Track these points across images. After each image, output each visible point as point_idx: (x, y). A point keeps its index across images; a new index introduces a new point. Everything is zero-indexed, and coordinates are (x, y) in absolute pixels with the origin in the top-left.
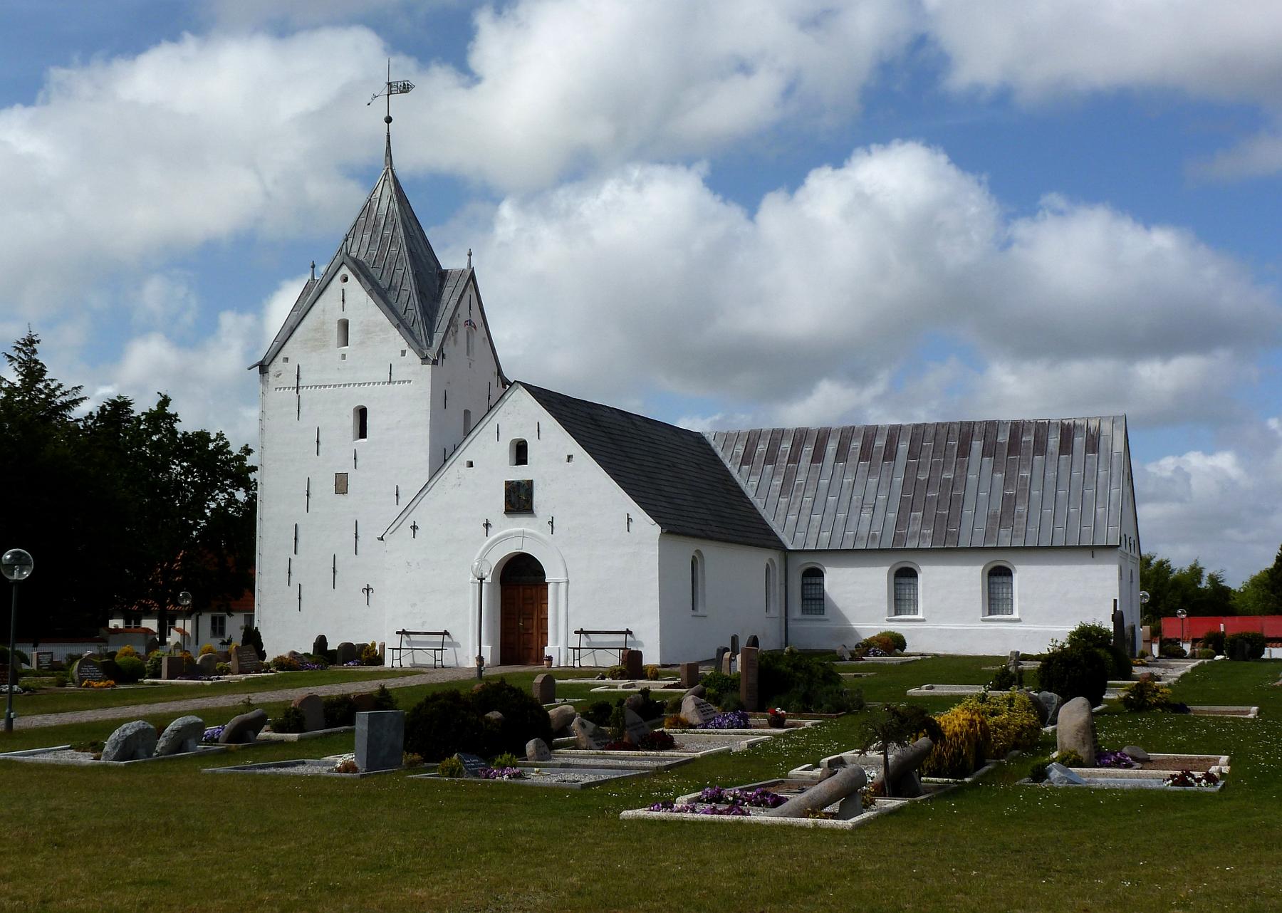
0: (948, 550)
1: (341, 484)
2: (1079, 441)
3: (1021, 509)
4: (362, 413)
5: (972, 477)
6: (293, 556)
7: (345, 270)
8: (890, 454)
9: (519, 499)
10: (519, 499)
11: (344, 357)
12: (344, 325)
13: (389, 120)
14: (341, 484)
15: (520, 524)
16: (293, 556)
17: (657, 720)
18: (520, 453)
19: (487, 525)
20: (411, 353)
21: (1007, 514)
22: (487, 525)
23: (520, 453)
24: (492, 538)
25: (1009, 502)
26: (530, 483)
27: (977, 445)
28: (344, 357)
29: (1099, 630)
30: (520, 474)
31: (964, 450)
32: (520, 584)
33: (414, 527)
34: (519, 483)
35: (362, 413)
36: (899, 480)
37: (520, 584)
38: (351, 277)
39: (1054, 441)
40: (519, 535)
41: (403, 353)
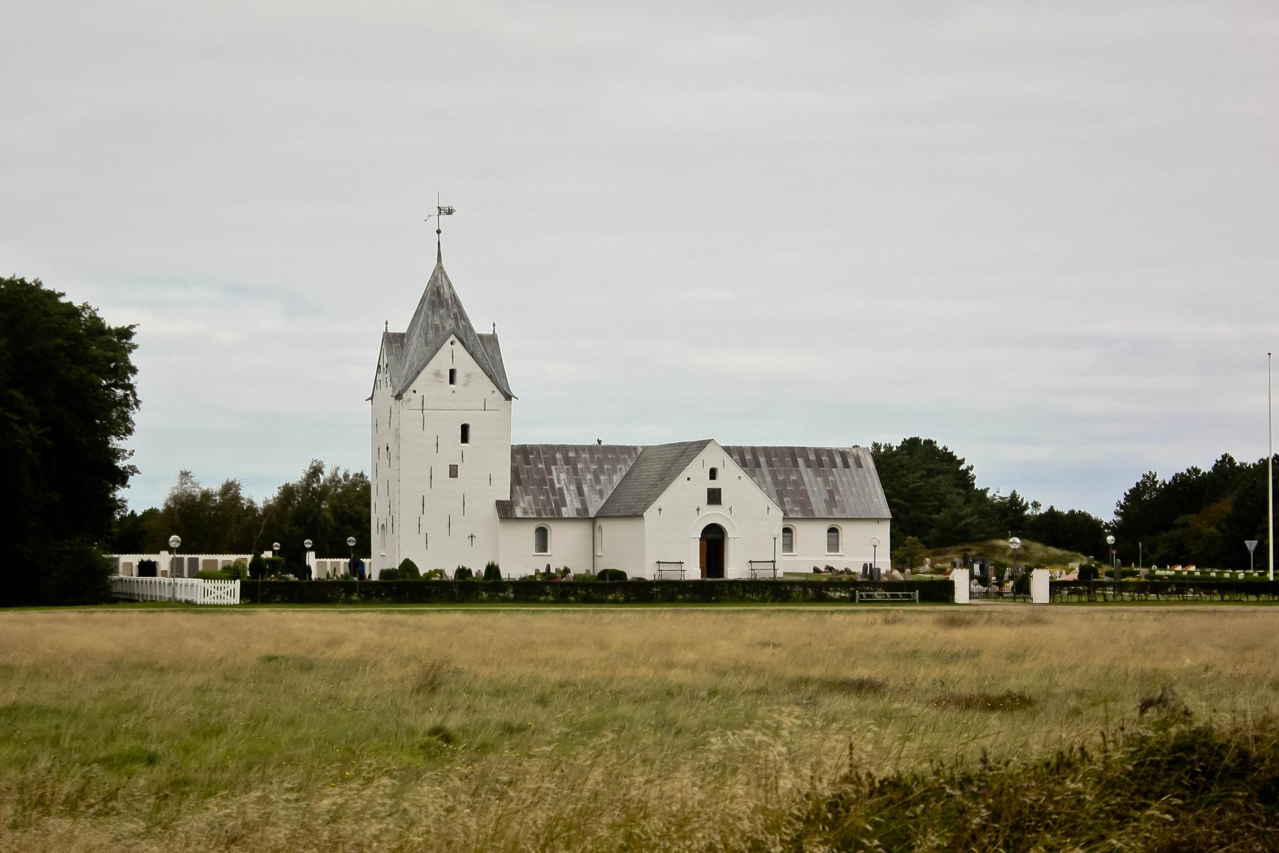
0: (810, 517)
1: (453, 471)
2: (851, 461)
3: (837, 498)
4: (465, 429)
5: (806, 479)
7: (453, 338)
8: (758, 465)
9: (714, 497)
10: (714, 497)
12: (452, 372)
13: (439, 232)
14: (453, 471)
15: (715, 509)
18: (713, 474)
20: (497, 392)
21: (831, 502)
23: (713, 474)
25: (831, 493)
27: (800, 461)
29: (416, 570)
31: (796, 465)
32: (713, 541)
35: (465, 429)
36: (769, 479)
37: (713, 541)
38: (457, 342)
39: (838, 460)
40: (714, 515)
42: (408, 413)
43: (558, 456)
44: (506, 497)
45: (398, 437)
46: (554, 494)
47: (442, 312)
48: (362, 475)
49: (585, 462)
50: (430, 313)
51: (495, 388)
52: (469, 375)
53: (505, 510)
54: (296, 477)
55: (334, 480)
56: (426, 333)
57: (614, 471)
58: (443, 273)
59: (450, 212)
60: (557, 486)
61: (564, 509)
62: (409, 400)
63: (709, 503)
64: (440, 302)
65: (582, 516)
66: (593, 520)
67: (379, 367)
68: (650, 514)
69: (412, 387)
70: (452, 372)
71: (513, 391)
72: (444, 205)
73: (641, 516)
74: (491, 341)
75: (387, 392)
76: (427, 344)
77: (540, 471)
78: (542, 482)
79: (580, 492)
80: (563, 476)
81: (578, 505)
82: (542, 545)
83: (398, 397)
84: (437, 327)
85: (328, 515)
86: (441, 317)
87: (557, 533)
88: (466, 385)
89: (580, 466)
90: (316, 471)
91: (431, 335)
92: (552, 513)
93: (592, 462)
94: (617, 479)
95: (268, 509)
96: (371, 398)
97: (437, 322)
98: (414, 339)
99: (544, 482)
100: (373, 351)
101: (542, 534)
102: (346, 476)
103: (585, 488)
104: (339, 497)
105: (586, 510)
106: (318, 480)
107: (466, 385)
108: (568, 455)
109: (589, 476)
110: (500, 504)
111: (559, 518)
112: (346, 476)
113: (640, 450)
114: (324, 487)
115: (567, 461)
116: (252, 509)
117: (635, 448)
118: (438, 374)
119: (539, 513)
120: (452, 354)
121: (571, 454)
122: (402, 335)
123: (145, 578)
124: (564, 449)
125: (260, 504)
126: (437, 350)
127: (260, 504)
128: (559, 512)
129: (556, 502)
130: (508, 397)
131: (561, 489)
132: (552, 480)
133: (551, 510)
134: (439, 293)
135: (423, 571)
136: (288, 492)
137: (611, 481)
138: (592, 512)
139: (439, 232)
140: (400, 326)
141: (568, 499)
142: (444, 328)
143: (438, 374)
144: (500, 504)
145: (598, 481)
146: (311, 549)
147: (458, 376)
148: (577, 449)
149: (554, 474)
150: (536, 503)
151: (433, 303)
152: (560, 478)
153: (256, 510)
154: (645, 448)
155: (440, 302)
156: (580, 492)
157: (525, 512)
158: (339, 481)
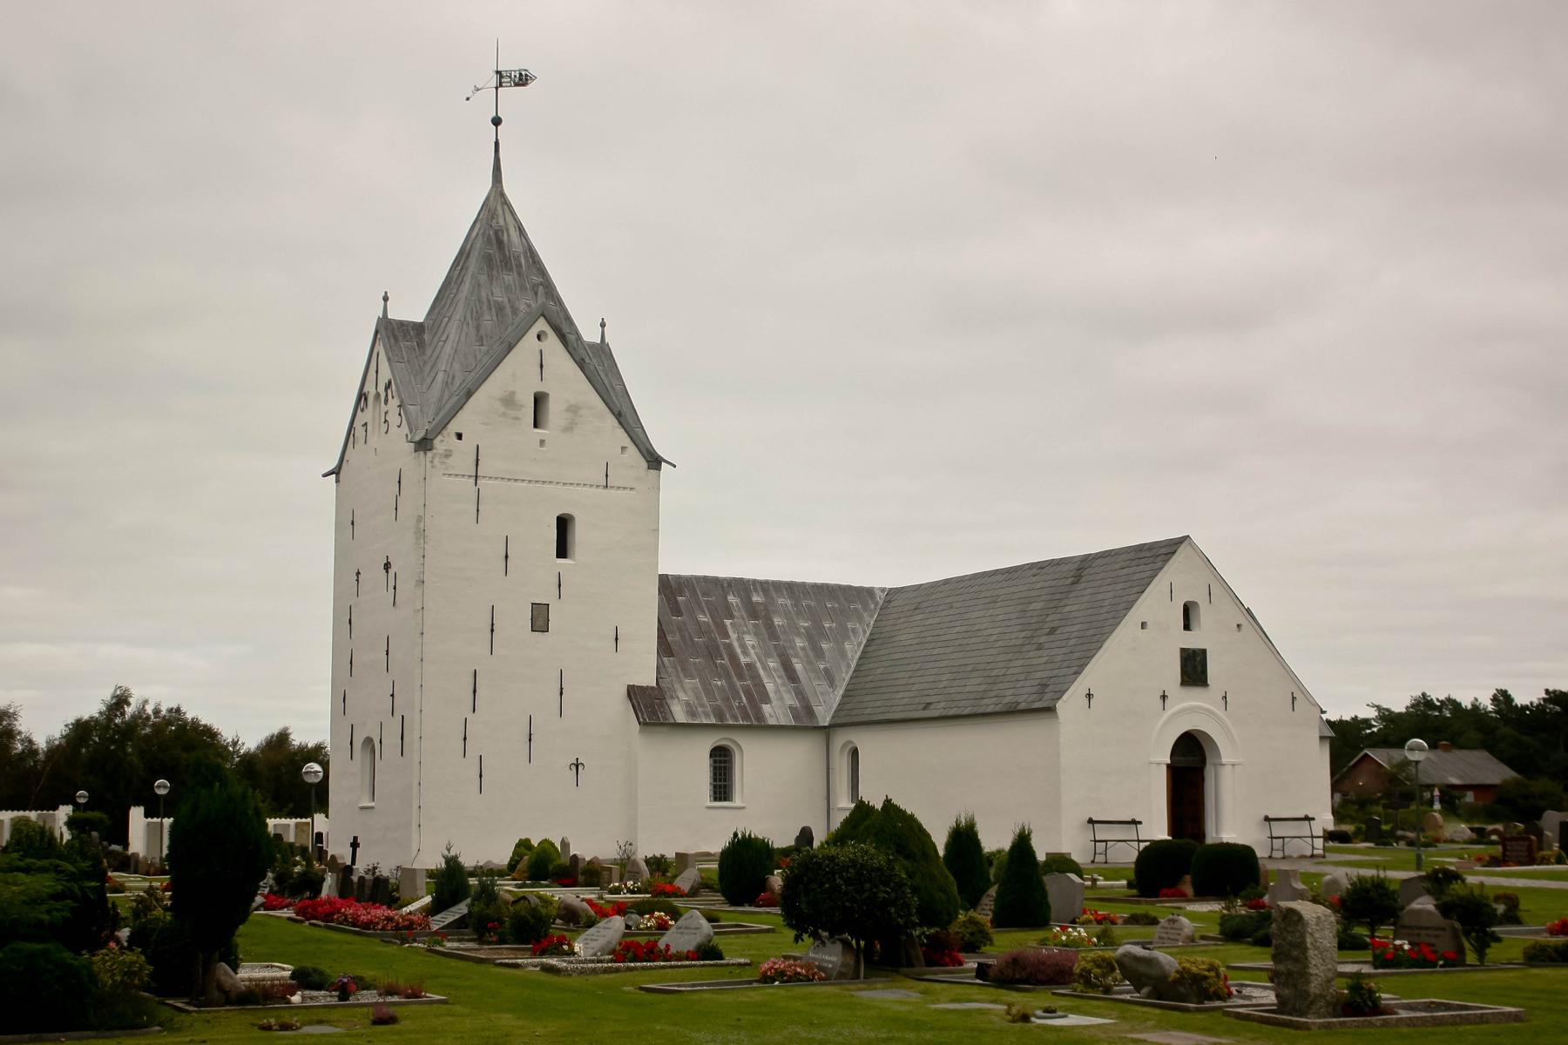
1: (540, 619)
4: (564, 524)
6: (470, 716)
7: (541, 325)
9: (1194, 669)
10: (1194, 669)
11: (542, 442)
12: (539, 400)
13: (497, 122)
14: (540, 619)
15: (1194, 698)
16: (470, 716)
17: (629, 939)
19: (1164, 697)
20: (632, 449)
22: (1164, 697)
24: (1169, 712)
26: (1204, 651)
28: (542, 442)
30: (1193, 641)
32: (1190, 764)
33: (1089, 696)
34: (1194, 651)
35: (564, 524)
40: (1192, 710)
41: (623, 448)
42: (445, 481)
43: (732, 599)
44: (648, 679)
45: (421, 534)
46: (741, 677)
47: (509, 278)
48: (178, 710)
49: (787, 614)
50: (483, 278)
51: (627, 442)
52: (574, 409)
53: (648, 706)
54: (91, 707)
55: (140, 717)
56: (478, 318)
57: (843, 634)
58: (506, 203)
59: (523, 80)
60: (743, 660)
61: (766, 708)
62: (448, 454)
63: (1184, 683)
64: (500, 270)
65: (804, 724)
66: (827, 731)
67: (362, 396)
68: (1069, 705)
69: (454, 427)
70: (539, 400)
71: (660, 451)
72: (510, 65)
73: (1050, 710)
74: (603, 350)
75: (394, 443)
76: (481, 340)
77: (701, 629)
78: (712, 652)
79: (791, 675)
80: (750, 640)
81: (790, 700)
82: (722, 788)
83: (424, 445)
84: (500, 309)
85: (135, 760)
86: (508, 288)
87: (757, 762)
88: (568, 429)
89: (777, 621)
90: (120, 701)
91: (488, 321)
92: (746, 716)
93: (799, 613)
94: (853, 650)
95: (53, 751)
96: (336, 472)
97: (500, 297)
98: (453, 330)
99: (714, 652)
100: (349, 354)
101: (722, 761)
102: (157, 712)
103: (798, 667)
104: (147, 738)
105: (810, 712)
106: (123, 714)
107: (568, 429)
108: (757, 600)
109: (799, 643)
110: (635, 694)
111: (759, 727)
112: (157, 712)
113: (880, 598)
114: (133, 716)
115: (753, 612)
116: (31, 750)
117: (870, 592)
118: (509, 401)
119: (720, 715)
120: (534, 362)
121: (756, 598)
122: (419, 328)
123: (772, 695)
124: (742, 586)
125: (41, 743)
126: (510, 348)
127: (41, 743)
128: (760, 716)
129: (748, 693)
130: (655, 462)
131: (750, 666)
132: (729, 647)
133: (742, 708)
134: (500, 242)
135: (535, 843)
136: (81, 730)
137: (842, 653)
138: (824, 717)
139: (497, 122)
140: (413, 308)
141: (770, 687)
142: (515, 311)
143: (509, 401)
144: (635, 694)
145: (819, 654)
146: (77, 806)
147: (554, 408)
148: (767, 587)
149: (733, 636)
150: (709, 692)
151: (488, 259)
152: (747, 644)
153: (36, 752)
154: (893, 593)
155: (500, 270)
156: (791, 675)
157: (692, 712)
158: (148, 718)
